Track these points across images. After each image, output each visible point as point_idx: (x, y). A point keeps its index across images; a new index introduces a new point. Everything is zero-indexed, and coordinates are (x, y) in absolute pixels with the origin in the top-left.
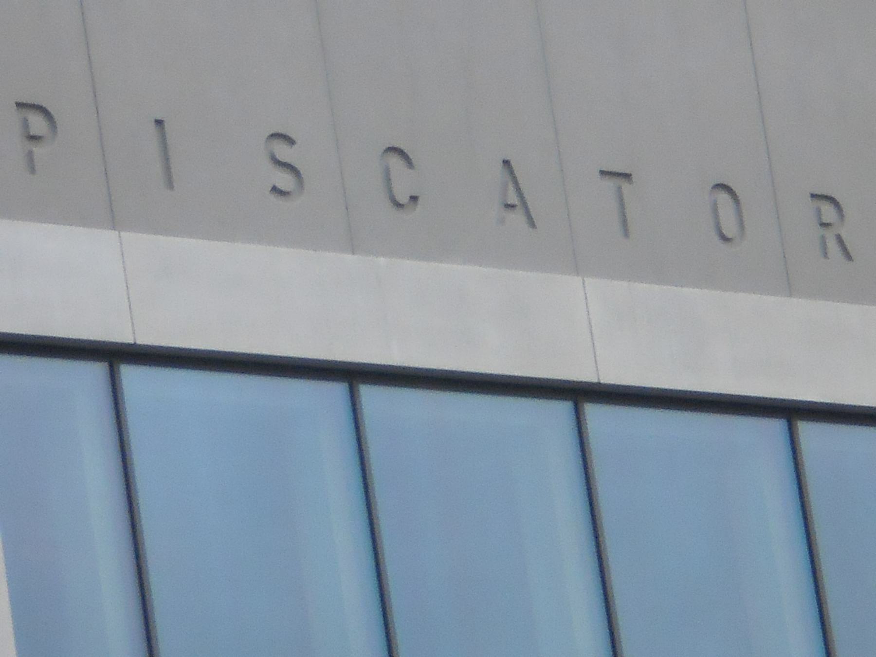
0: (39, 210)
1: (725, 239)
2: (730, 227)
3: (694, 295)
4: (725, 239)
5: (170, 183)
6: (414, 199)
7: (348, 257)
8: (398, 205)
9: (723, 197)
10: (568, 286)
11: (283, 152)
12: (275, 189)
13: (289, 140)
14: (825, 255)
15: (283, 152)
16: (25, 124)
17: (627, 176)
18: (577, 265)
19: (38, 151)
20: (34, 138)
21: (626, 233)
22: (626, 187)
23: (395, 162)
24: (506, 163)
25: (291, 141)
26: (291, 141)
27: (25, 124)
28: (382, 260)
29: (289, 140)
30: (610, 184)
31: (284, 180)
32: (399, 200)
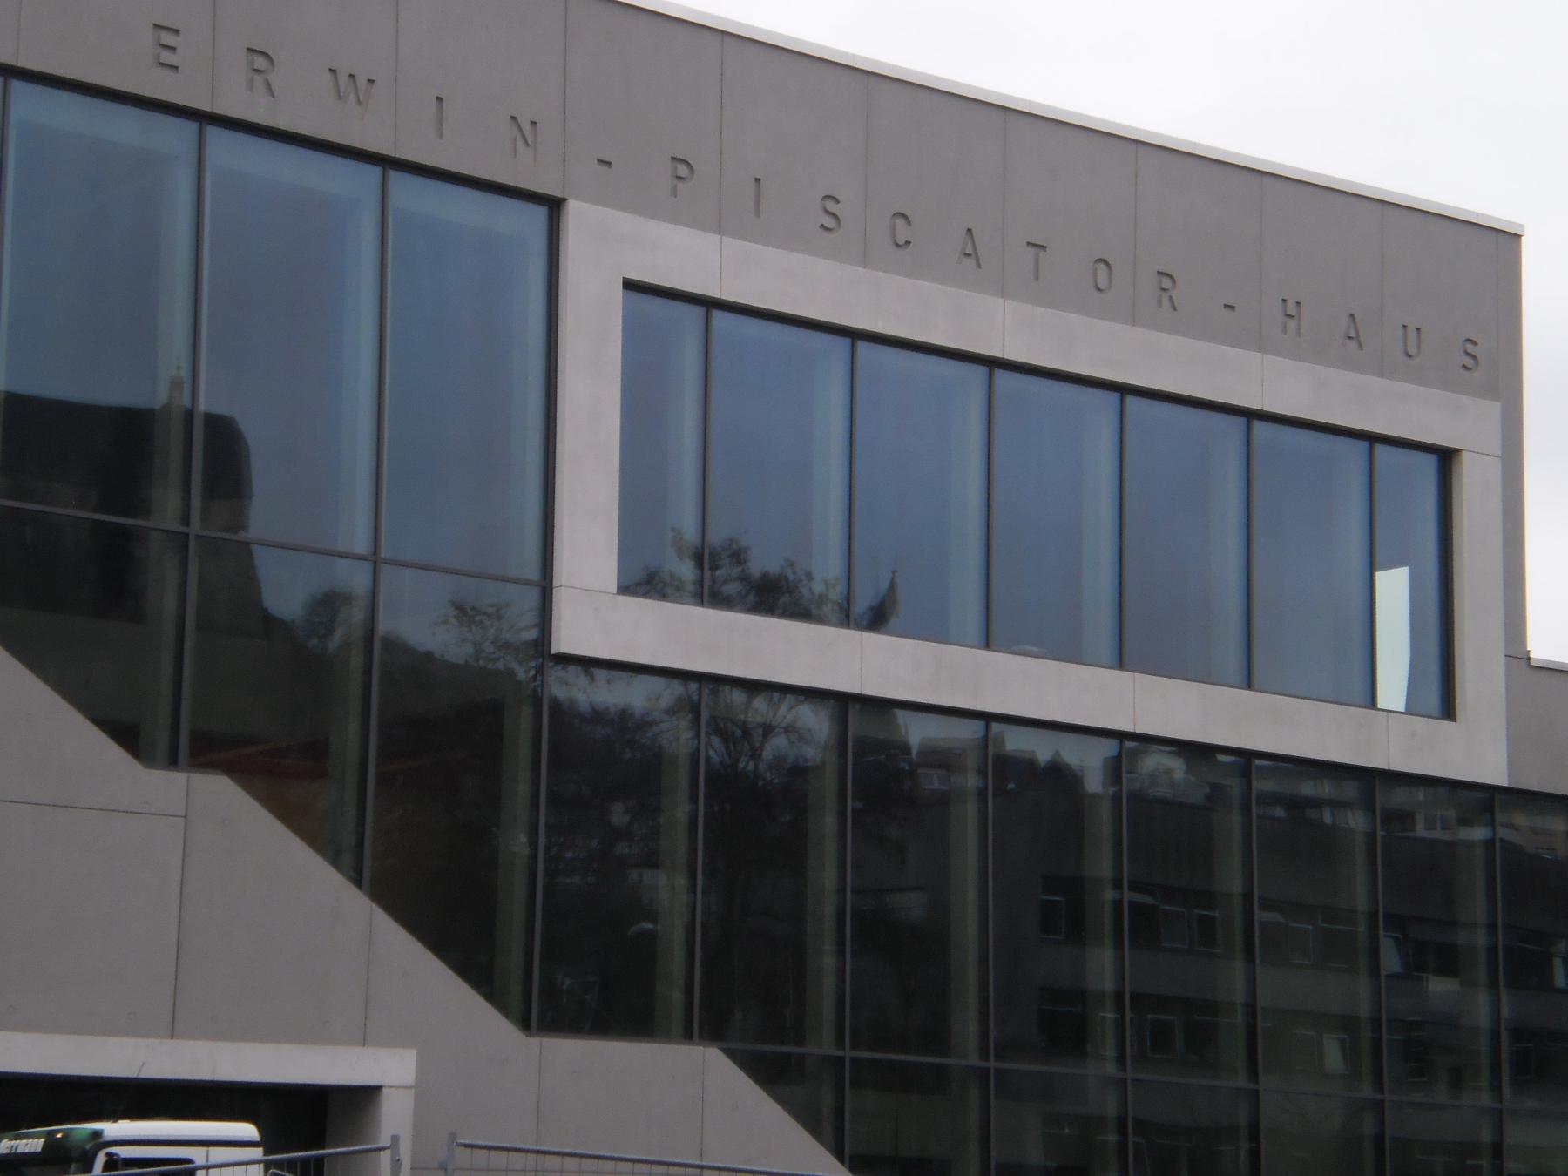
0: (674, 218)
1: (1099, 290)
2: (1102, 284)
3: (1072, 318)
4: (1099, 290)
5: (758, 213)
6: (908, 243)
7: (861, 269)
8: (897, 245)
9: (1102, 266)
10: (995, 304)
11: (831, 206)
12: (822, 226)
13: (1474, 343)
14: (175, 68)
15: (831, 206)
16: (1160, 282)
17: (1044, 247)
18: (1002, 293)
19: (681, 185)
20: (680, 178)
21: (1037, 278)
22: (1042, 253)
23: (900, 222)
24: (969, 230)
25: (837, 201)
26: (837, 201)
27: (1160, 282)
28: (881, 274)
29: (1474, 343)
30: (1032, 250)
31: (829, 222)
32: (898, 242)
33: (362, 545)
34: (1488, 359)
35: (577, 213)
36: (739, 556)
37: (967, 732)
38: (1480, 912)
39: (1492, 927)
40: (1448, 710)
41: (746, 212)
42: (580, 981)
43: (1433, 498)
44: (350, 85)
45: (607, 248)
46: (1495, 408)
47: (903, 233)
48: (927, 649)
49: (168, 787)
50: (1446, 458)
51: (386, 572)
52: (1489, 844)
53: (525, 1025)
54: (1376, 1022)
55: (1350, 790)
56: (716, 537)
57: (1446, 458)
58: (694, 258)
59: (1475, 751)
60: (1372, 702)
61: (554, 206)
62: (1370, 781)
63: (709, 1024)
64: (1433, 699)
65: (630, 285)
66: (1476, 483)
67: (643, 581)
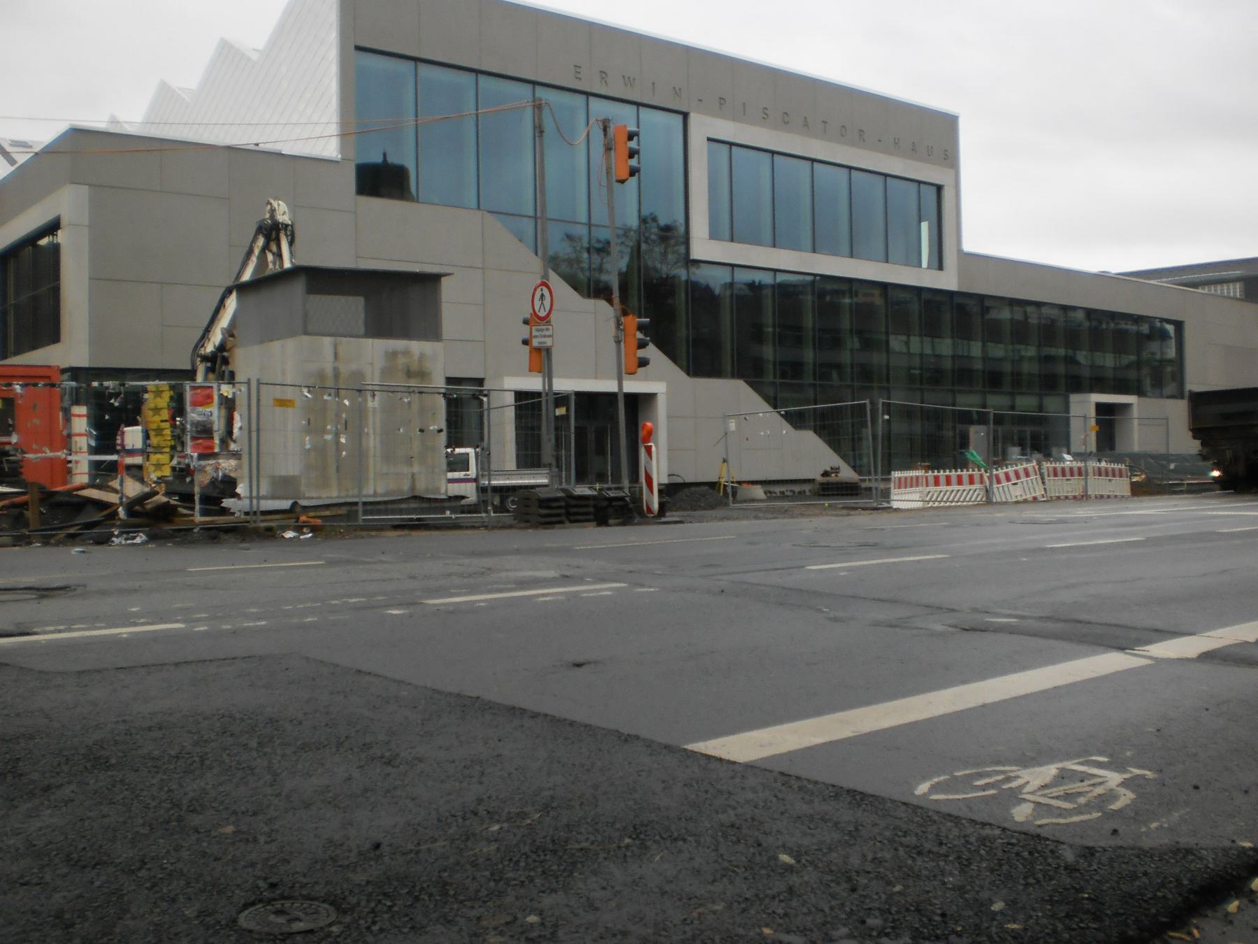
32: (784, 122)
33: (584, 219)
34: (950, 158)
35: (694, 118)
36: (655, 219)
37: (810, 278)
38: (770, 321)
39: (774, 326)
40: (941, 267)
41: (740, 114)
42: (701, 360)
43: (936, 202)
44: (629, 81)
45: (703, 126)
46: (952, 171)
47: (786, 119)
48: (793, 253)
49: (591, 302)
50: (939, 188)
51: (593, 229)
52: (851, 304)
53: (688, 374)
54: (852, 365)
55: (845, 287)
56: (645, 213)
57: (939, 188)
58: (727, 129)
59: (948, 281)
60: (920, 266)
61: (685, 116)
62: (918, 290)
63: (738, 373)
64: (936, 264)
65: (709, 139)
66: (947, 195)
67: (714, 235)
